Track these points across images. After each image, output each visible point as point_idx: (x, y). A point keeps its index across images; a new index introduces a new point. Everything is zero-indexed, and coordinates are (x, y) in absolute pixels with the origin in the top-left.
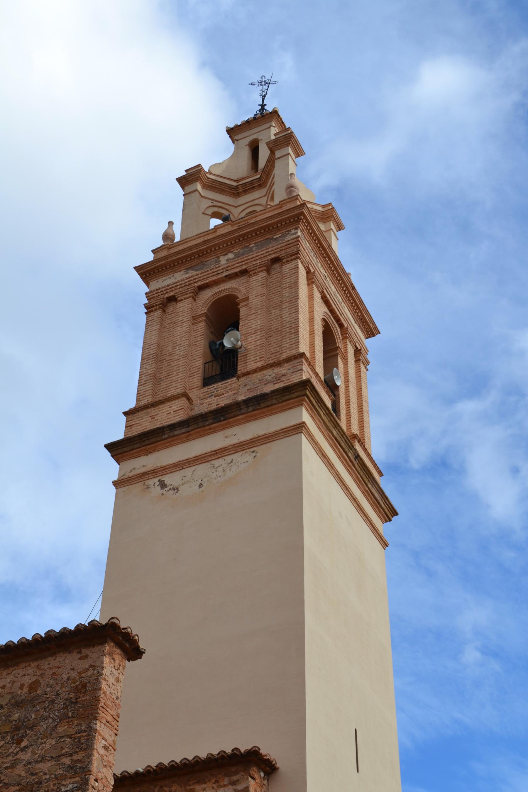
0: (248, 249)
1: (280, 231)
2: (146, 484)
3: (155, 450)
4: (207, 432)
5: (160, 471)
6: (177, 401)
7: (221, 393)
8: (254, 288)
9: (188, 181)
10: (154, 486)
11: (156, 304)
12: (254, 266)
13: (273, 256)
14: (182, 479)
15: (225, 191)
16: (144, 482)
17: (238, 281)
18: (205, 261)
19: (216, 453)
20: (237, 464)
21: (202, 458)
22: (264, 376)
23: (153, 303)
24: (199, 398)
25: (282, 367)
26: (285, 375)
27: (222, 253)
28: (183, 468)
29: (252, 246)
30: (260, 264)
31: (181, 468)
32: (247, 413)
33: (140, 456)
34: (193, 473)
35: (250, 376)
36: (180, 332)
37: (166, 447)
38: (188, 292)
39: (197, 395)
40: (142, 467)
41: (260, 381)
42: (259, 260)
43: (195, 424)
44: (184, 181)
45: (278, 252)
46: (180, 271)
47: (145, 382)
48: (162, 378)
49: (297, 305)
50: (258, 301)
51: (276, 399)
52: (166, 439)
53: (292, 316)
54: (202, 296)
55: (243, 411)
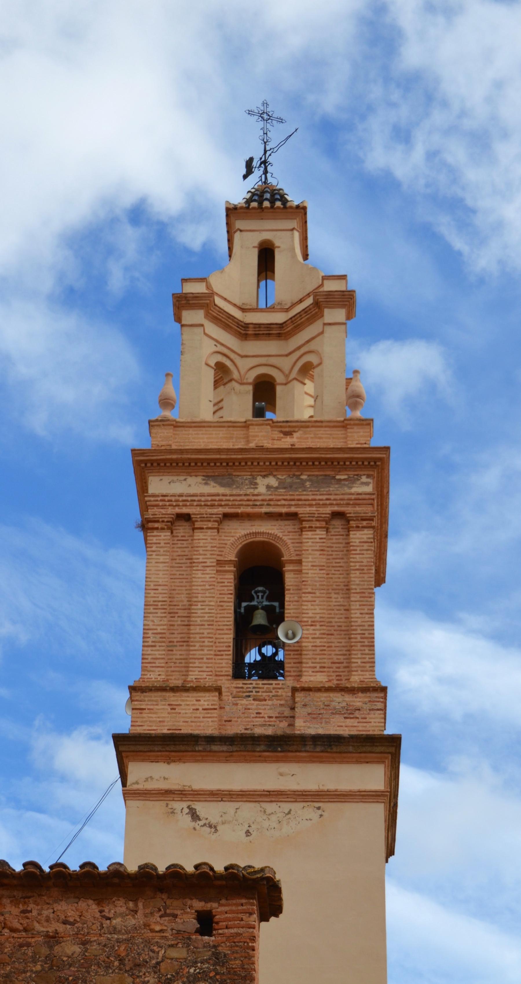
0: (299, 481)
1: (346, 471)
2: (170, 806)
3: (180, 759)
4: (254, 759)
5: (190, 794)
6: (207, 694)
7: (262, 698)
8: (310, 551)
9: (189, 304)
10: (182, 812)
11: (163, 519)
12: (310, 515)
13: (336, 509)
14: (222, 816)
15: (231, 327)
16: (168, 802)
17: (281, 526)
18: (235, 475)
19: (270, 795)
20: (297, 818)
21: (249, 795)
22: (331, 701)
23: (158, 516)
24: (231, 694)
25: (355, 695)
26: (359, 710)
27: (260, 472)
28: (222, 800)
29: (304, 477)
30: (319, 515)
31: (220, 799)
32: (313, 752)
33: (158, 762)
34: (236, 812)
35: (311, 693)
36: (202, 582)
37: (196, 761)
38: (212, 519)
39: (228, 688)
40: (162, 779)
41: (325, 706)
42: (315, 506)
43: (241, 745)
44: (183, 302)
45: (343, 504)
46: (196, 476)
47: (153, 644)
48: (173, 642)
49: (371, 603)
50: (316, 575)
51: (353, 746)
52: (199, 751)
53: (365, 618)
54: (228, 529)
55: (308, 748)
